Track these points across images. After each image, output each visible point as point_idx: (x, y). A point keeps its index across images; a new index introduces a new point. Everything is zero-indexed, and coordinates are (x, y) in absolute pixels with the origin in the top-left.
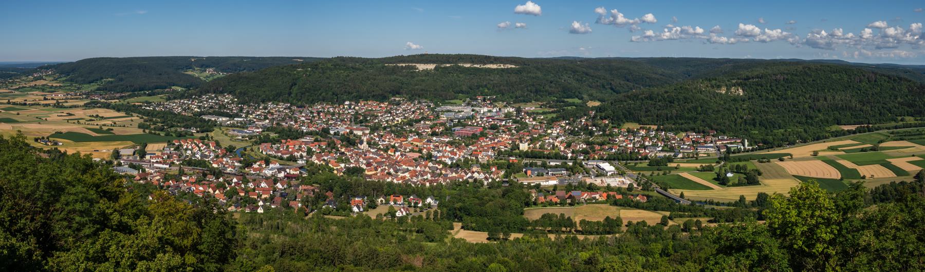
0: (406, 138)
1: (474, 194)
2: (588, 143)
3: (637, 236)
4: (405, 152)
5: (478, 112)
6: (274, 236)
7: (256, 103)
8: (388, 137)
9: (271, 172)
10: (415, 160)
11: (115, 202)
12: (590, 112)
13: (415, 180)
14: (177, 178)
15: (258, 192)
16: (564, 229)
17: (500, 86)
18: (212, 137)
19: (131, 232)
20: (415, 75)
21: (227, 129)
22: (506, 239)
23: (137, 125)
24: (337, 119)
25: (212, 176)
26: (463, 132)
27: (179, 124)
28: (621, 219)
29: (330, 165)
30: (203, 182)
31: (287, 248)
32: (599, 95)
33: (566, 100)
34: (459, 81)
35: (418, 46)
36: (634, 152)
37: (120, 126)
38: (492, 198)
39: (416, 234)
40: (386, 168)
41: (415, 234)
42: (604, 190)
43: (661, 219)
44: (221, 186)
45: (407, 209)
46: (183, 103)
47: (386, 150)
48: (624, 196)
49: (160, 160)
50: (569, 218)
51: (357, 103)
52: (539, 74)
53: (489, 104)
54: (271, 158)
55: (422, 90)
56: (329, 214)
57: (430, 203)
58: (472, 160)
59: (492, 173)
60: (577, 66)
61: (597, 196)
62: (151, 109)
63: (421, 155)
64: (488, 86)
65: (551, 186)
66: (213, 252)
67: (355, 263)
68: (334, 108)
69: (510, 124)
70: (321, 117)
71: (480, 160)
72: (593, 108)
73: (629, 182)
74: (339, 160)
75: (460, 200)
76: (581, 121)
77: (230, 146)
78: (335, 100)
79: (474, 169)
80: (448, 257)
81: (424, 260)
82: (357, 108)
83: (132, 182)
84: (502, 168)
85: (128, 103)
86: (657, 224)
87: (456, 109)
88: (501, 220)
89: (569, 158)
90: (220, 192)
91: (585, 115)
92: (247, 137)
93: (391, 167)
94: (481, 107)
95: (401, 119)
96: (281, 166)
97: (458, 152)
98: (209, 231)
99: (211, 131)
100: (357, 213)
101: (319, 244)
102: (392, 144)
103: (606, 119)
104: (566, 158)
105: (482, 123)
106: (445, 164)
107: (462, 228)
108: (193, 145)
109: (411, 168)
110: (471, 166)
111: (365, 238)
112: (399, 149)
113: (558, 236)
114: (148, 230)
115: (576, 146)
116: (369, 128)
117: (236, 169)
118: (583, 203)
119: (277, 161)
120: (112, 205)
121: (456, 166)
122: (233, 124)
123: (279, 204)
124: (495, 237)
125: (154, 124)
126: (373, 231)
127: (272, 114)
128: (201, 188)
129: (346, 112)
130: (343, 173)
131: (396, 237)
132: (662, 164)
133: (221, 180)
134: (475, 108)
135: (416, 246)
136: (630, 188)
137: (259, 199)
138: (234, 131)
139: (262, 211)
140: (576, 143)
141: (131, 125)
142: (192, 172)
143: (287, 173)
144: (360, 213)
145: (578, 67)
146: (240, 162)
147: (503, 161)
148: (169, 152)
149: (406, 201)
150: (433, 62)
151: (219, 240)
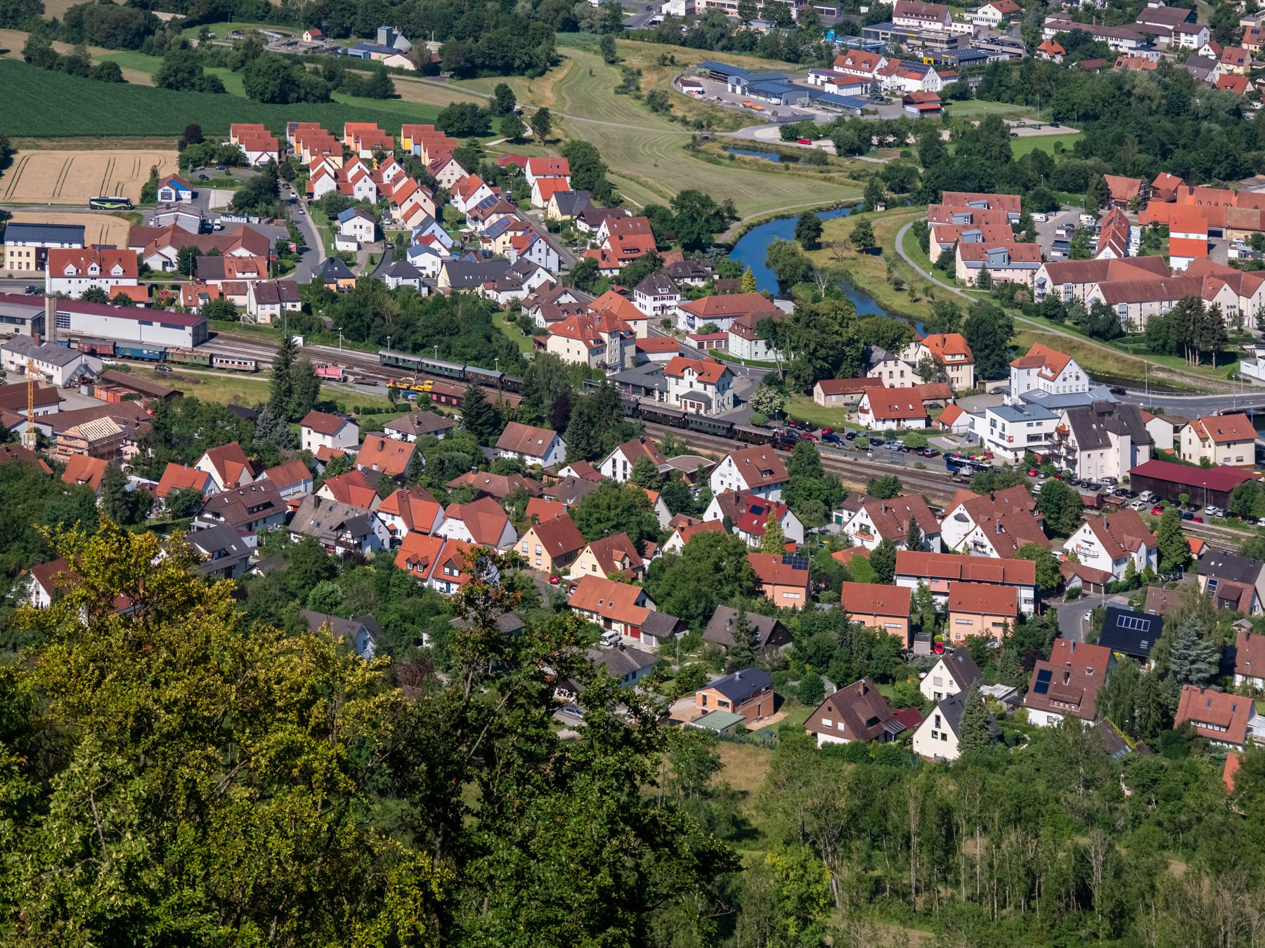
9: (1020, 432)
15: (912, 584)
18: (542, 120)
25: (547, 433)
30: (470, 478)
49: (118, 281)
54: (1019, 318)
77: (685, 195)
96: (1103, 394)
98: (521, 878)
99: (536, 68)
108: (392, 170)
117: (738, 385)
123: (1089, 706)
128: (455, 530)
137: (922, 648)
138: (719, 74)
139: (950, 750)
142: (379, 393)
143: (1155, 455)
146: (771, 332)
148: (190, 224)
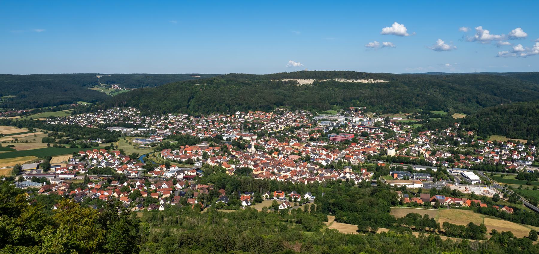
0: (288, 142)
1: (346, 192)
2: (452, 152)
3: (501, 245)
4: (287, 155)
5: (350, 121)
6: (174, 230)
7: (158, 115)
8: (272, 142)
9: (171, 174)
10: (296, 161)
11: (17, 217)
12: (456, 124)
13: (295, 178)
14: (82, 186)
15: (159, 192)
16: (427, 229)
17: (371, 98)
18: (117, 147)
19: (34, 243)
20: (296, 88)
21: (131, 139)
22: (374, 233)
23: (41, 139)
24: (229, 127)
26: (339, 138)
27: (85, 137)
28: (486, 227)
29: (222, 166)
30: (108, 188)
31: (185, 239)
32: (465, 108)
33: (431, 112)
34: (334, 94)
35: (299, 64)
36: (500, 164)
37: (23, 142)
38: (362, 196)
39: (296, 224)
40: (271, 168)
41: (294, 224)
42: (468, 197)
43: (530, 233)
44: (125, 190)
45: (288, 203)
46: (89, 117)
47: (271, 153)
48: (489, 205)
49: (65, 171)
50: (433, 219)
51: (246, 112)
52: (406, 88)
53: (360, 114)
54: (171, 162)
55: (302, 102)
56: (222, 208)
57: (307, 199)
58: (345, 163)
59: (362, 174)
60: (443, 81)
61: (461, 202)
62: (56, 123)
63: (300, 157)
64: (360, 98)
65: (416, 189)
66: (118, 250)
67: (244, 249)
68: (226, 117)
69: (379, 132)
70: (216, 125)
71: (352, 162)
72: (458, 120)
73: (494, 193)
74: (230, 162)
75: (334, 197)
76: (446, 132)
78: (228, 111)
79: (347, 170)
80: (322, 244)
81: (302, 246)
82: (246, 117)
83: (35, 195)
84: (371, 171)
85: (31, 119)
86: (525, 237)
87: (331, 118)
88: (370, 216)
89: (434, 165)
90: (124, 195)
91: (450, 126)
92: (149, 145)
93: (275, 167)
94: (353, 117)
95: (284, 126)
96: (180, 169)
97: (332, 156)
99: (116, 141)
100: (246, 206)
101: (213, 234)
102: (276, 148)
103: (471, 130)
104: (431, 165)
105: (354, 130)
106: (321, 166)
107: (336, 220)
108: (99, 154)
109: (291, 168)
110: (344, 167)
111: (252, 227)
112: (282, 152)
113: (421, 234)
114: (52, 239)
115: (441, 154)
116: (256, 134)
117: (139, 173)
118: (446, 207)
119: (176, 165)
120: (13, 221)
121: (330, 167)
122: (137, 133)
124: (364, 229)
125: (60, 137)
126: (259, 222)
127: (172, 124)
128: (106, 194)
129: (237, 121)
130: (234, 173)
131: (278, 227)
132: (532, 178)
133: (125, 184)
134: (348, 118)
135: (295, 234)
136: (496, 198)
138: (137, 140)
140: (441, 152)
141: (35, 140)
142: (97, 180)
143: (185, 175)
144: (248, 207)
145: (444, 82)
146: (143, 167)
147: (372, 164)
148: (74, 163)
149: (287, 197)
150: (312, 78)
151: (124, 238)
